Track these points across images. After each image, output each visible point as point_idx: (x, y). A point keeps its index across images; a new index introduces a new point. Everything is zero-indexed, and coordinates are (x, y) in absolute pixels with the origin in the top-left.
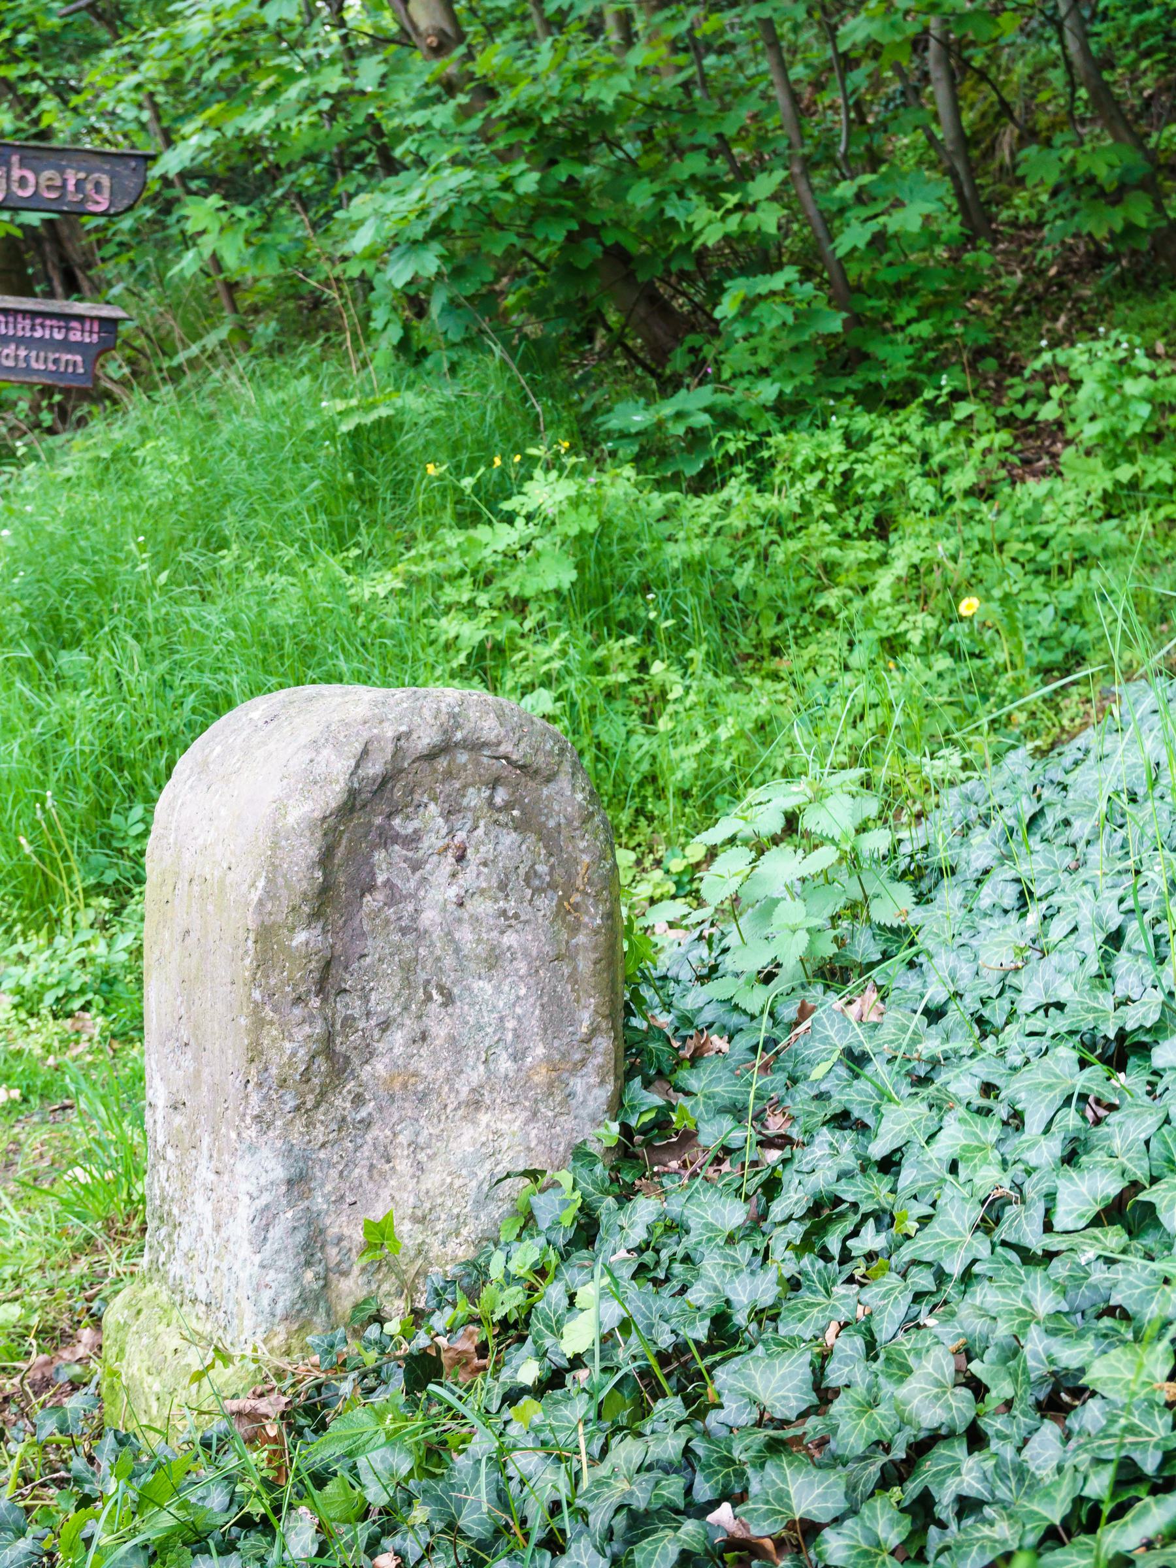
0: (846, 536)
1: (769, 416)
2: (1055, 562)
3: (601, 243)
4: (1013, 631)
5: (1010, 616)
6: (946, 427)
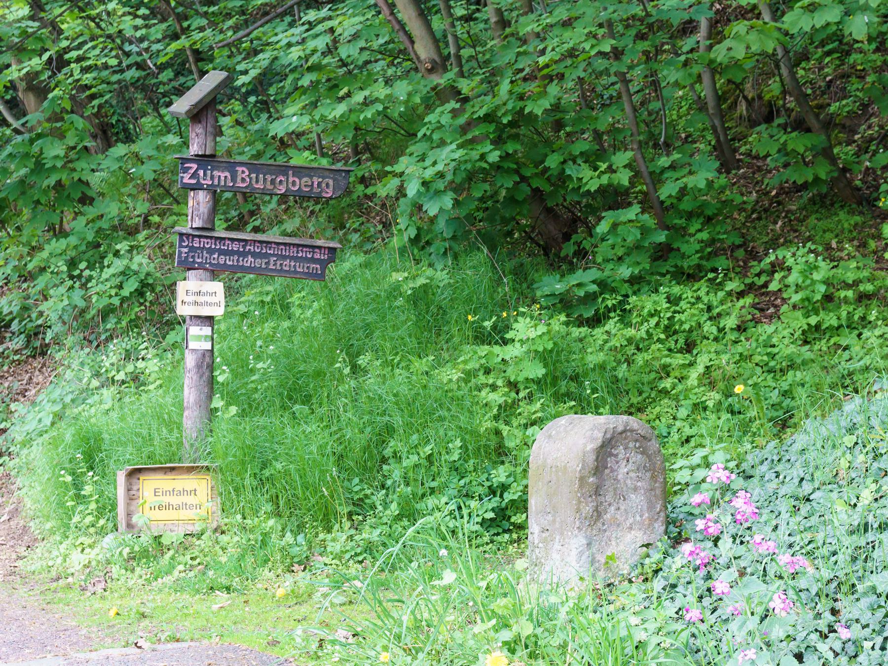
0: (670, 350)
1: (626, 285)
2: (778, 367)
3: (529, 185)
4: (759, 401)
5: (757, 394)
6: (721, 294)
